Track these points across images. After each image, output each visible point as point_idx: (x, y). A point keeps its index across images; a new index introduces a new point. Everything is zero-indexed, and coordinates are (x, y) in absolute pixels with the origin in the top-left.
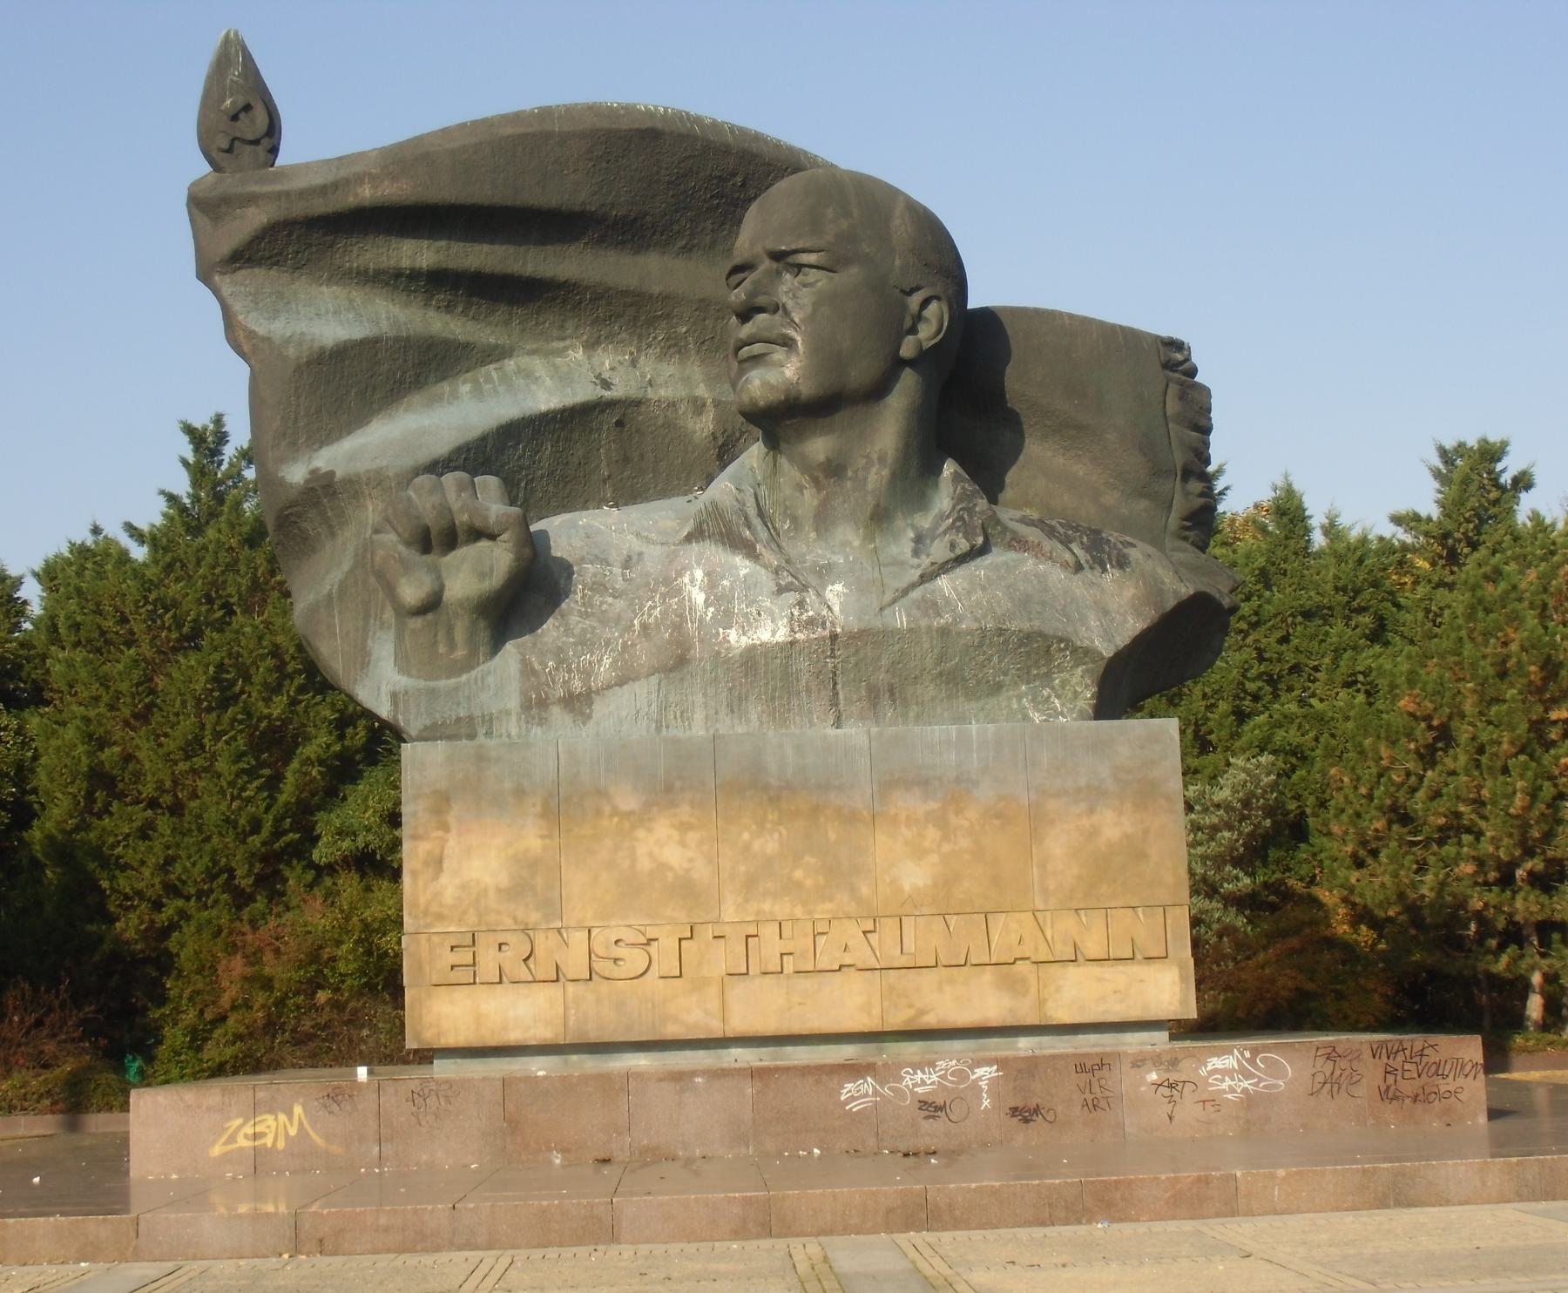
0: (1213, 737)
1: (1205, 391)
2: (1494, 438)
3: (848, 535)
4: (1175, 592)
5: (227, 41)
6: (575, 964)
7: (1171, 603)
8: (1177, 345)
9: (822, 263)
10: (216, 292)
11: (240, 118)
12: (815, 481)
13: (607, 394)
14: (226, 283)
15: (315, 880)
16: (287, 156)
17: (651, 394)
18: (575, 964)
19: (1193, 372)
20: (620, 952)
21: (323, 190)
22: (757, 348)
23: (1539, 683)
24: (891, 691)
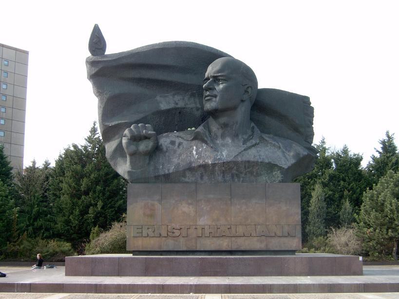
1: (312, 109)
2: (32, 160)
3: (229, 140)
4: (303, 154)
5: (95, 26)
6: (164, 233)
7: (301, 156)
9: (224, 79)
11: (97, 42)
12: (222, 127)
13: (177, 106)
16: (107, 53)
17: (187, 106)
18: (164, 233)
20: (174, 231)
23: (156, 165)
24: (237, 175)
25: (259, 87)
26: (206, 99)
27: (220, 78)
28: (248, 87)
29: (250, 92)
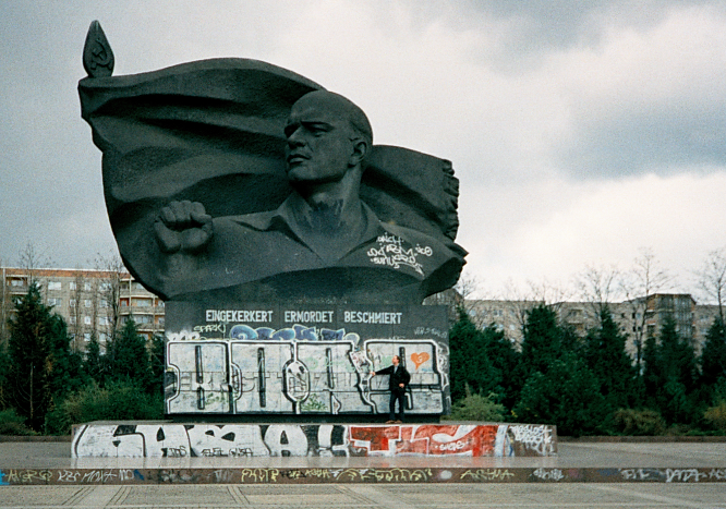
0: (109, 279)
1: (457, 180)
8: (449, 163)
10: (90, 124)
11: (98, 52)
14: (97, 122)
15: (430, 387)
16: (115, 73)
19: (453, 173)
21: (132, 88)
22: (299, 159)
25: (375, 143)
26: (292, 161)
27: (318, 126)
28: (360, 144)
29: (363, 151)
